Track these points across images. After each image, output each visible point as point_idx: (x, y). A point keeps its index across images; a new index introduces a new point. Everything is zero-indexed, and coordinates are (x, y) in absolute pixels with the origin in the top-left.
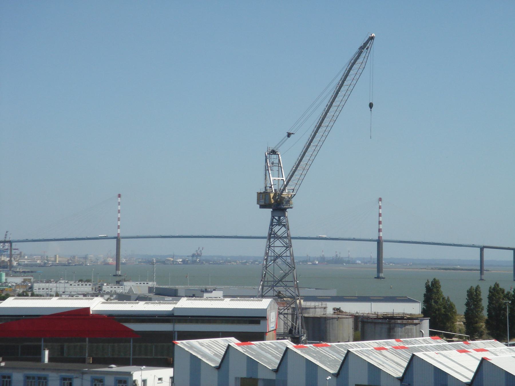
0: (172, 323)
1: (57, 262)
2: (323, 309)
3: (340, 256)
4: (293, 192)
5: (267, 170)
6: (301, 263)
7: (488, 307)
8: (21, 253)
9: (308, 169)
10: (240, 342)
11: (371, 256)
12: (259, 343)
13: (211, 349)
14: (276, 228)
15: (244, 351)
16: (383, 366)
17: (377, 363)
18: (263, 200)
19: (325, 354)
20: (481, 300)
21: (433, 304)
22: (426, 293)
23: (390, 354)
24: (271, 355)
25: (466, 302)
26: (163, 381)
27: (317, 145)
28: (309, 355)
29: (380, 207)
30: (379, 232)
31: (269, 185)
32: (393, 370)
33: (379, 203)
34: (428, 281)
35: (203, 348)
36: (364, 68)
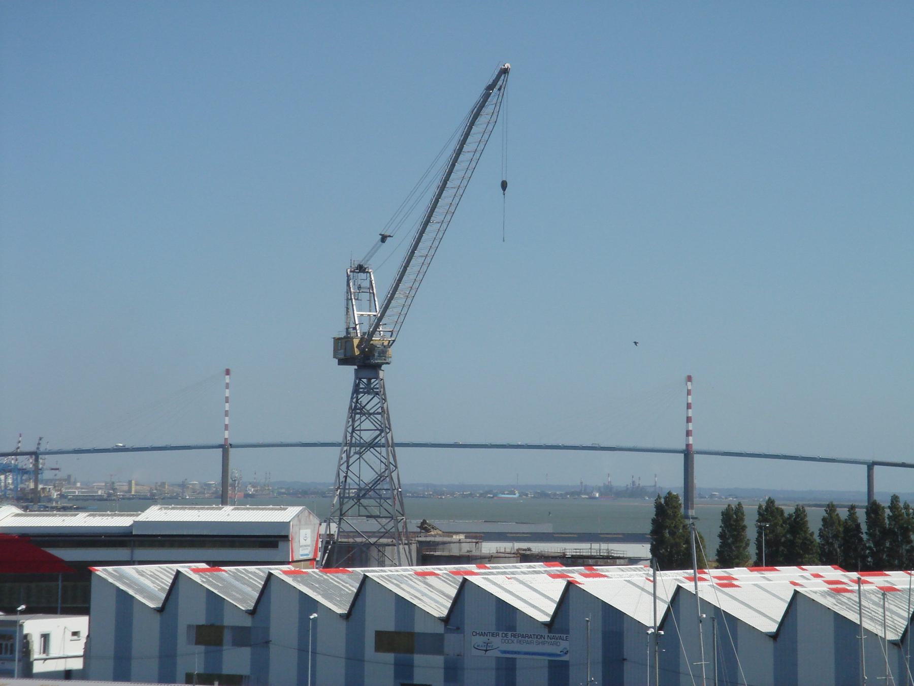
0: (129, 548)
1: (133, 493)
2: (475, 543)
3: (639, 484)
4: (391, 336)
5: (349, 300)
6: (568, 496)
7: (756, 541)
8: (69, 476)
9: (414, 297)
10: (208, 567)
11: (485, 522)
12: (235, 569)
13: (157, 581)
14: (364, 399)
15: (203, 581)
16: (420, 599)
17: (413, 595)
18: (342, 351)
19: (338, 584)
20: (744, 528)
21: (667, 535)
22: (655, 517)
23: (442, 582)
24: (251, 587)
25: (720, 532)
26: (81, 638)
27: (427, 255)
28: (304, 585)
29: (689, 393)
30: (687, 436)
31: (352, 325)
32: (436, 606)
33: (686, 384)
34: (659, 496)
35: (142, 580)
36: (496, 122)
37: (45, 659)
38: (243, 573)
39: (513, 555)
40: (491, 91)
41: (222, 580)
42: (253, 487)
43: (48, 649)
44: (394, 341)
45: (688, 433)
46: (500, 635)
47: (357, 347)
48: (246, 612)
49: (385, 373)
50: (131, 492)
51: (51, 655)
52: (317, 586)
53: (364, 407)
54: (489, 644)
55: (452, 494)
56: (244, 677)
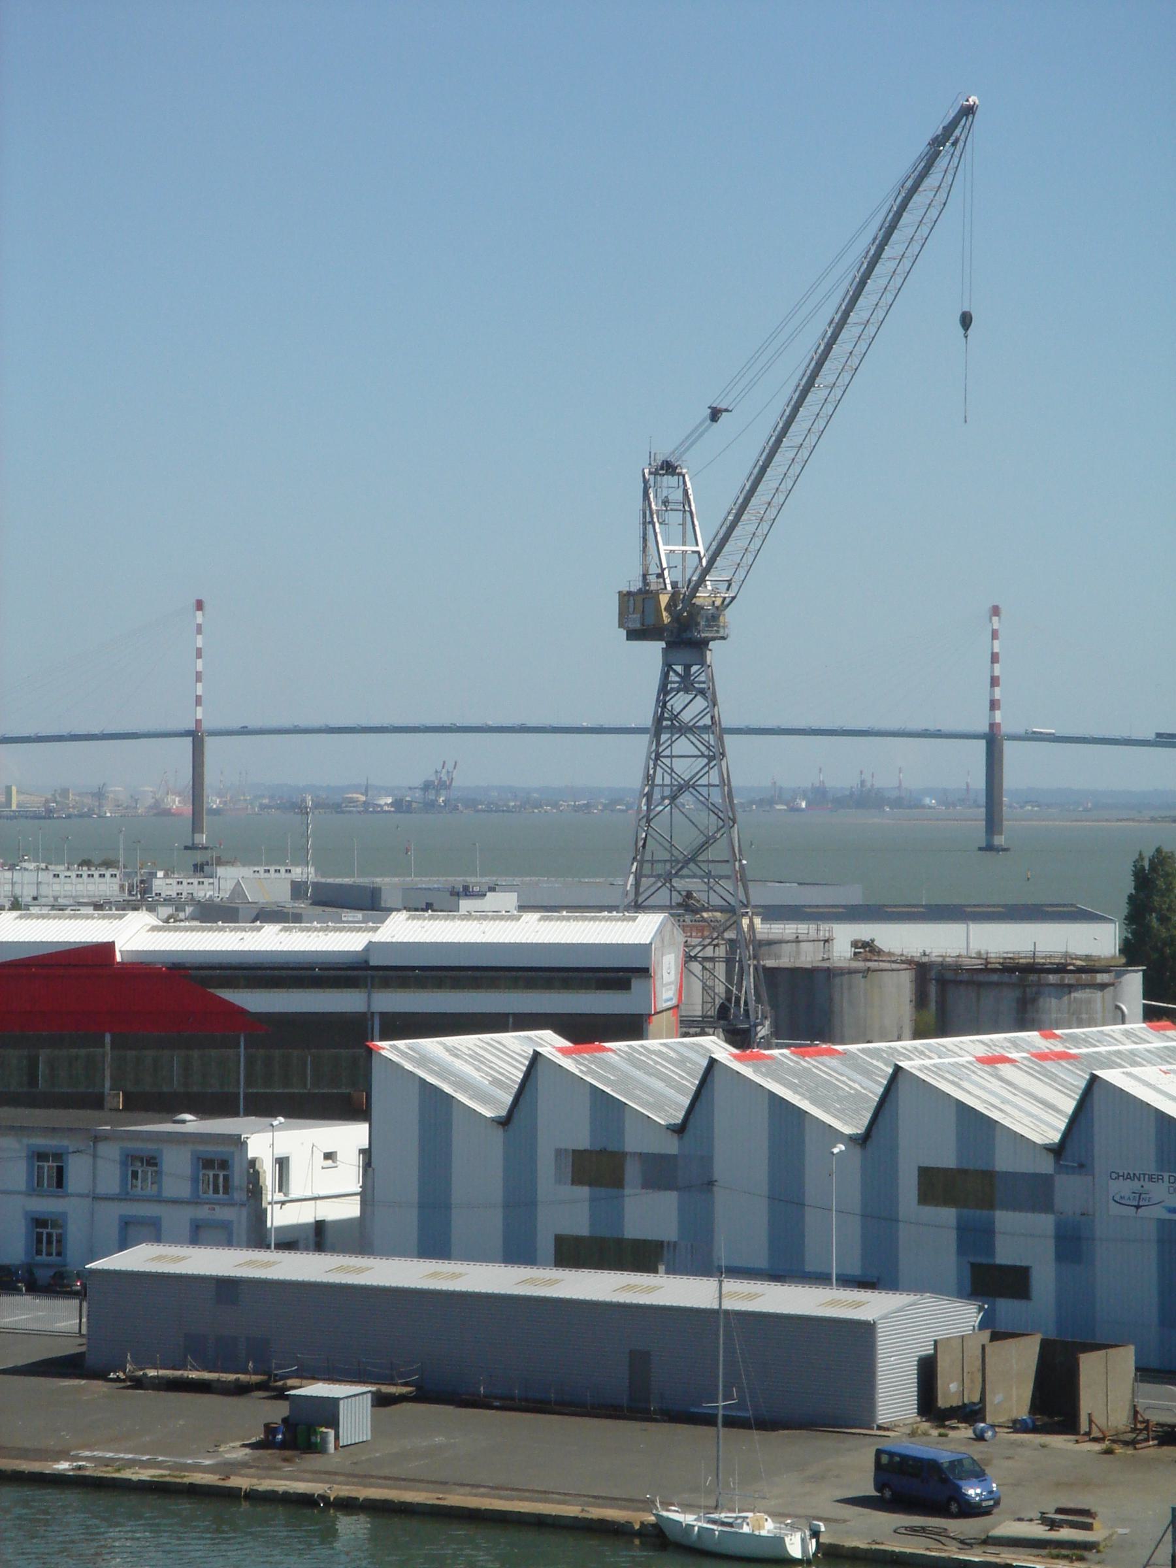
1: (14, 807)
4: (728, 589)
12: (628, 1046)
13: (483, 1067)
14: (678, 701)
15: (581, 1071)
16: (1001, 1110)
18: (637, 616)
19: (828, 1078)
21: (1155, 923)
22: (1133, 892)
26: (338, 1163)
27: (802, 445)
29: (995, 635)
32: (1032, 1122)
34: (1140, 854)
35: (459, 1065)
36: (945, 204)
37: (283, 1203)
38: (641, 1053)
39: (904, 966)
40: (942, 148)
41: (612, 1068)
42: (220, 795)
43: (288, 1184)
44: (733, 598)
45: (994, 705)
46: (1166, 1179)
47: (665, 609)
48: (668, 1128)
49: (716, 653)
50: (11, 807)
51: (292, 1196)
52: (796, 1081)
53: (676, 716)
54: (1143, 1196)
55: (555, 805)
56: (665, 1244)
